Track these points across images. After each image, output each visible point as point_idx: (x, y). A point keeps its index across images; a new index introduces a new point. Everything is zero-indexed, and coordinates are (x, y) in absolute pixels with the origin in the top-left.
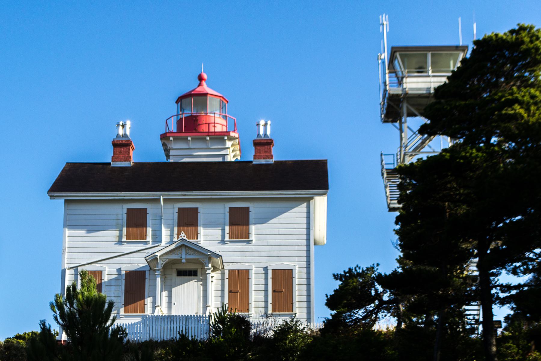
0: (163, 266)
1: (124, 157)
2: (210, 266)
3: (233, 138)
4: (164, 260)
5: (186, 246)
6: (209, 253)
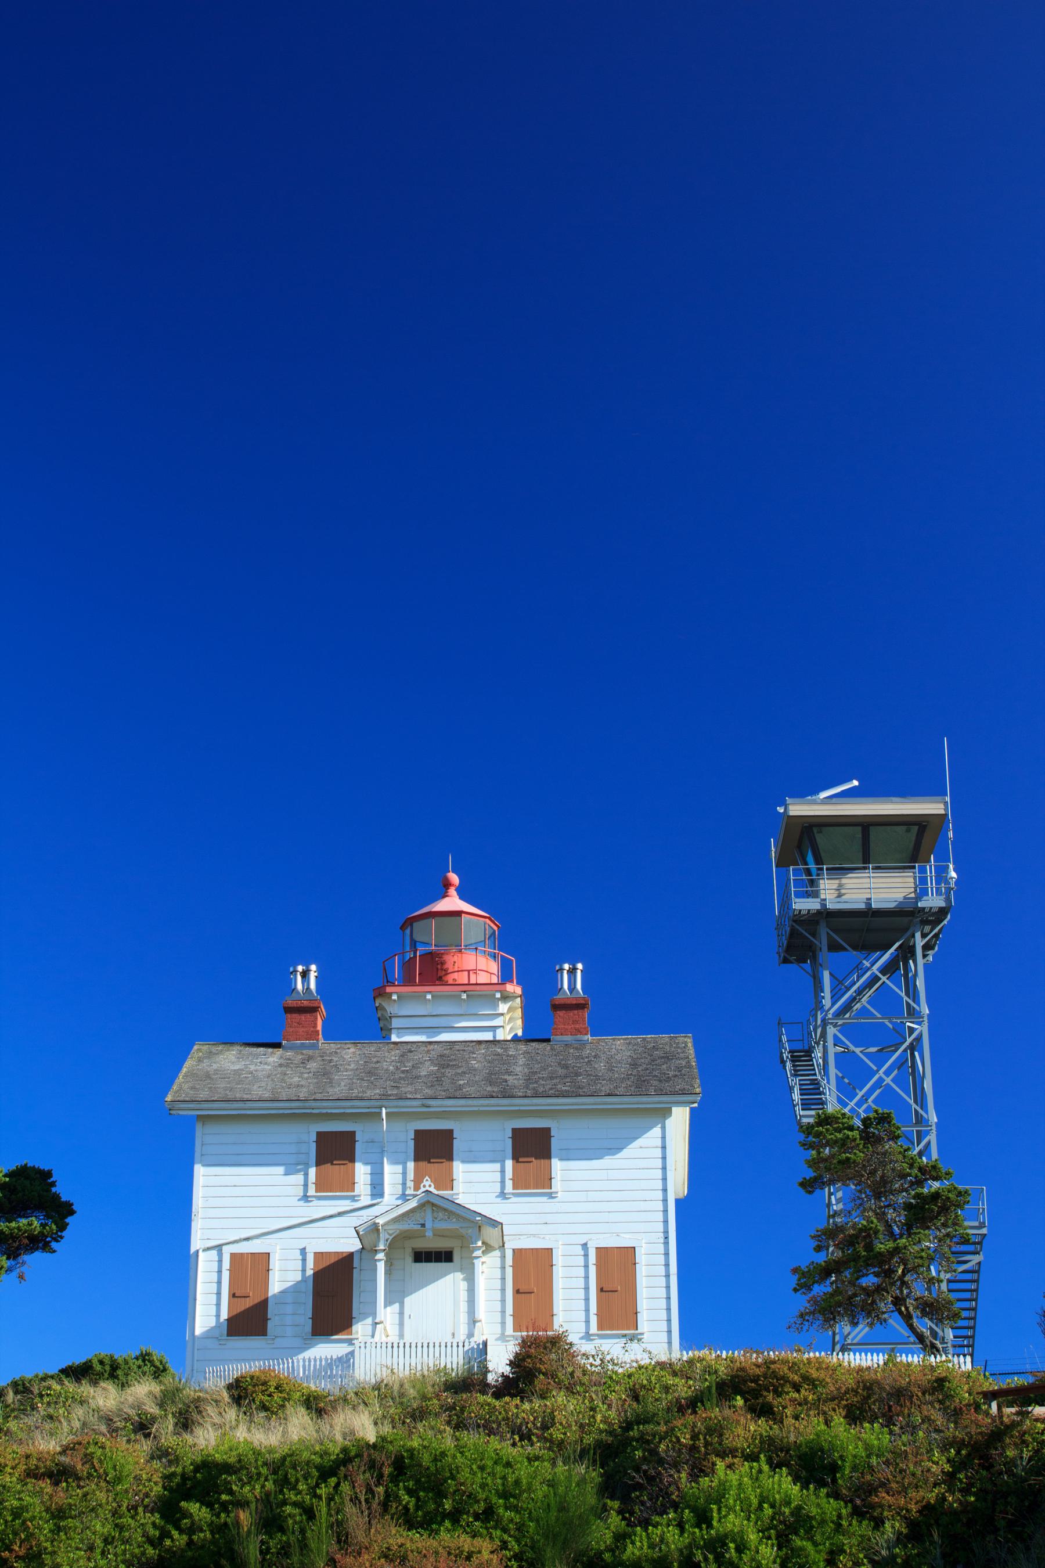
0: (390, 1244)
1: (307, 1032)
2: (480, 1243)
3: (511, 995)
4: (391, 1232)
5: (433, 1205)
6: (478, 1219)
